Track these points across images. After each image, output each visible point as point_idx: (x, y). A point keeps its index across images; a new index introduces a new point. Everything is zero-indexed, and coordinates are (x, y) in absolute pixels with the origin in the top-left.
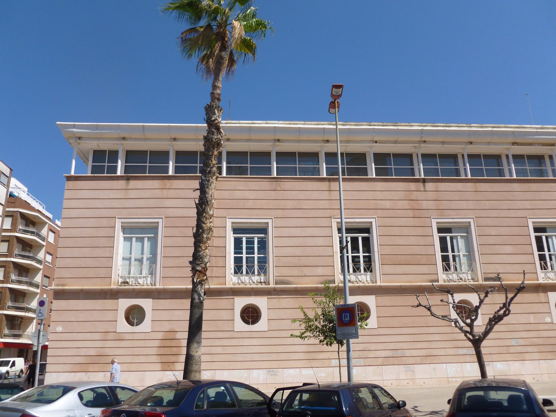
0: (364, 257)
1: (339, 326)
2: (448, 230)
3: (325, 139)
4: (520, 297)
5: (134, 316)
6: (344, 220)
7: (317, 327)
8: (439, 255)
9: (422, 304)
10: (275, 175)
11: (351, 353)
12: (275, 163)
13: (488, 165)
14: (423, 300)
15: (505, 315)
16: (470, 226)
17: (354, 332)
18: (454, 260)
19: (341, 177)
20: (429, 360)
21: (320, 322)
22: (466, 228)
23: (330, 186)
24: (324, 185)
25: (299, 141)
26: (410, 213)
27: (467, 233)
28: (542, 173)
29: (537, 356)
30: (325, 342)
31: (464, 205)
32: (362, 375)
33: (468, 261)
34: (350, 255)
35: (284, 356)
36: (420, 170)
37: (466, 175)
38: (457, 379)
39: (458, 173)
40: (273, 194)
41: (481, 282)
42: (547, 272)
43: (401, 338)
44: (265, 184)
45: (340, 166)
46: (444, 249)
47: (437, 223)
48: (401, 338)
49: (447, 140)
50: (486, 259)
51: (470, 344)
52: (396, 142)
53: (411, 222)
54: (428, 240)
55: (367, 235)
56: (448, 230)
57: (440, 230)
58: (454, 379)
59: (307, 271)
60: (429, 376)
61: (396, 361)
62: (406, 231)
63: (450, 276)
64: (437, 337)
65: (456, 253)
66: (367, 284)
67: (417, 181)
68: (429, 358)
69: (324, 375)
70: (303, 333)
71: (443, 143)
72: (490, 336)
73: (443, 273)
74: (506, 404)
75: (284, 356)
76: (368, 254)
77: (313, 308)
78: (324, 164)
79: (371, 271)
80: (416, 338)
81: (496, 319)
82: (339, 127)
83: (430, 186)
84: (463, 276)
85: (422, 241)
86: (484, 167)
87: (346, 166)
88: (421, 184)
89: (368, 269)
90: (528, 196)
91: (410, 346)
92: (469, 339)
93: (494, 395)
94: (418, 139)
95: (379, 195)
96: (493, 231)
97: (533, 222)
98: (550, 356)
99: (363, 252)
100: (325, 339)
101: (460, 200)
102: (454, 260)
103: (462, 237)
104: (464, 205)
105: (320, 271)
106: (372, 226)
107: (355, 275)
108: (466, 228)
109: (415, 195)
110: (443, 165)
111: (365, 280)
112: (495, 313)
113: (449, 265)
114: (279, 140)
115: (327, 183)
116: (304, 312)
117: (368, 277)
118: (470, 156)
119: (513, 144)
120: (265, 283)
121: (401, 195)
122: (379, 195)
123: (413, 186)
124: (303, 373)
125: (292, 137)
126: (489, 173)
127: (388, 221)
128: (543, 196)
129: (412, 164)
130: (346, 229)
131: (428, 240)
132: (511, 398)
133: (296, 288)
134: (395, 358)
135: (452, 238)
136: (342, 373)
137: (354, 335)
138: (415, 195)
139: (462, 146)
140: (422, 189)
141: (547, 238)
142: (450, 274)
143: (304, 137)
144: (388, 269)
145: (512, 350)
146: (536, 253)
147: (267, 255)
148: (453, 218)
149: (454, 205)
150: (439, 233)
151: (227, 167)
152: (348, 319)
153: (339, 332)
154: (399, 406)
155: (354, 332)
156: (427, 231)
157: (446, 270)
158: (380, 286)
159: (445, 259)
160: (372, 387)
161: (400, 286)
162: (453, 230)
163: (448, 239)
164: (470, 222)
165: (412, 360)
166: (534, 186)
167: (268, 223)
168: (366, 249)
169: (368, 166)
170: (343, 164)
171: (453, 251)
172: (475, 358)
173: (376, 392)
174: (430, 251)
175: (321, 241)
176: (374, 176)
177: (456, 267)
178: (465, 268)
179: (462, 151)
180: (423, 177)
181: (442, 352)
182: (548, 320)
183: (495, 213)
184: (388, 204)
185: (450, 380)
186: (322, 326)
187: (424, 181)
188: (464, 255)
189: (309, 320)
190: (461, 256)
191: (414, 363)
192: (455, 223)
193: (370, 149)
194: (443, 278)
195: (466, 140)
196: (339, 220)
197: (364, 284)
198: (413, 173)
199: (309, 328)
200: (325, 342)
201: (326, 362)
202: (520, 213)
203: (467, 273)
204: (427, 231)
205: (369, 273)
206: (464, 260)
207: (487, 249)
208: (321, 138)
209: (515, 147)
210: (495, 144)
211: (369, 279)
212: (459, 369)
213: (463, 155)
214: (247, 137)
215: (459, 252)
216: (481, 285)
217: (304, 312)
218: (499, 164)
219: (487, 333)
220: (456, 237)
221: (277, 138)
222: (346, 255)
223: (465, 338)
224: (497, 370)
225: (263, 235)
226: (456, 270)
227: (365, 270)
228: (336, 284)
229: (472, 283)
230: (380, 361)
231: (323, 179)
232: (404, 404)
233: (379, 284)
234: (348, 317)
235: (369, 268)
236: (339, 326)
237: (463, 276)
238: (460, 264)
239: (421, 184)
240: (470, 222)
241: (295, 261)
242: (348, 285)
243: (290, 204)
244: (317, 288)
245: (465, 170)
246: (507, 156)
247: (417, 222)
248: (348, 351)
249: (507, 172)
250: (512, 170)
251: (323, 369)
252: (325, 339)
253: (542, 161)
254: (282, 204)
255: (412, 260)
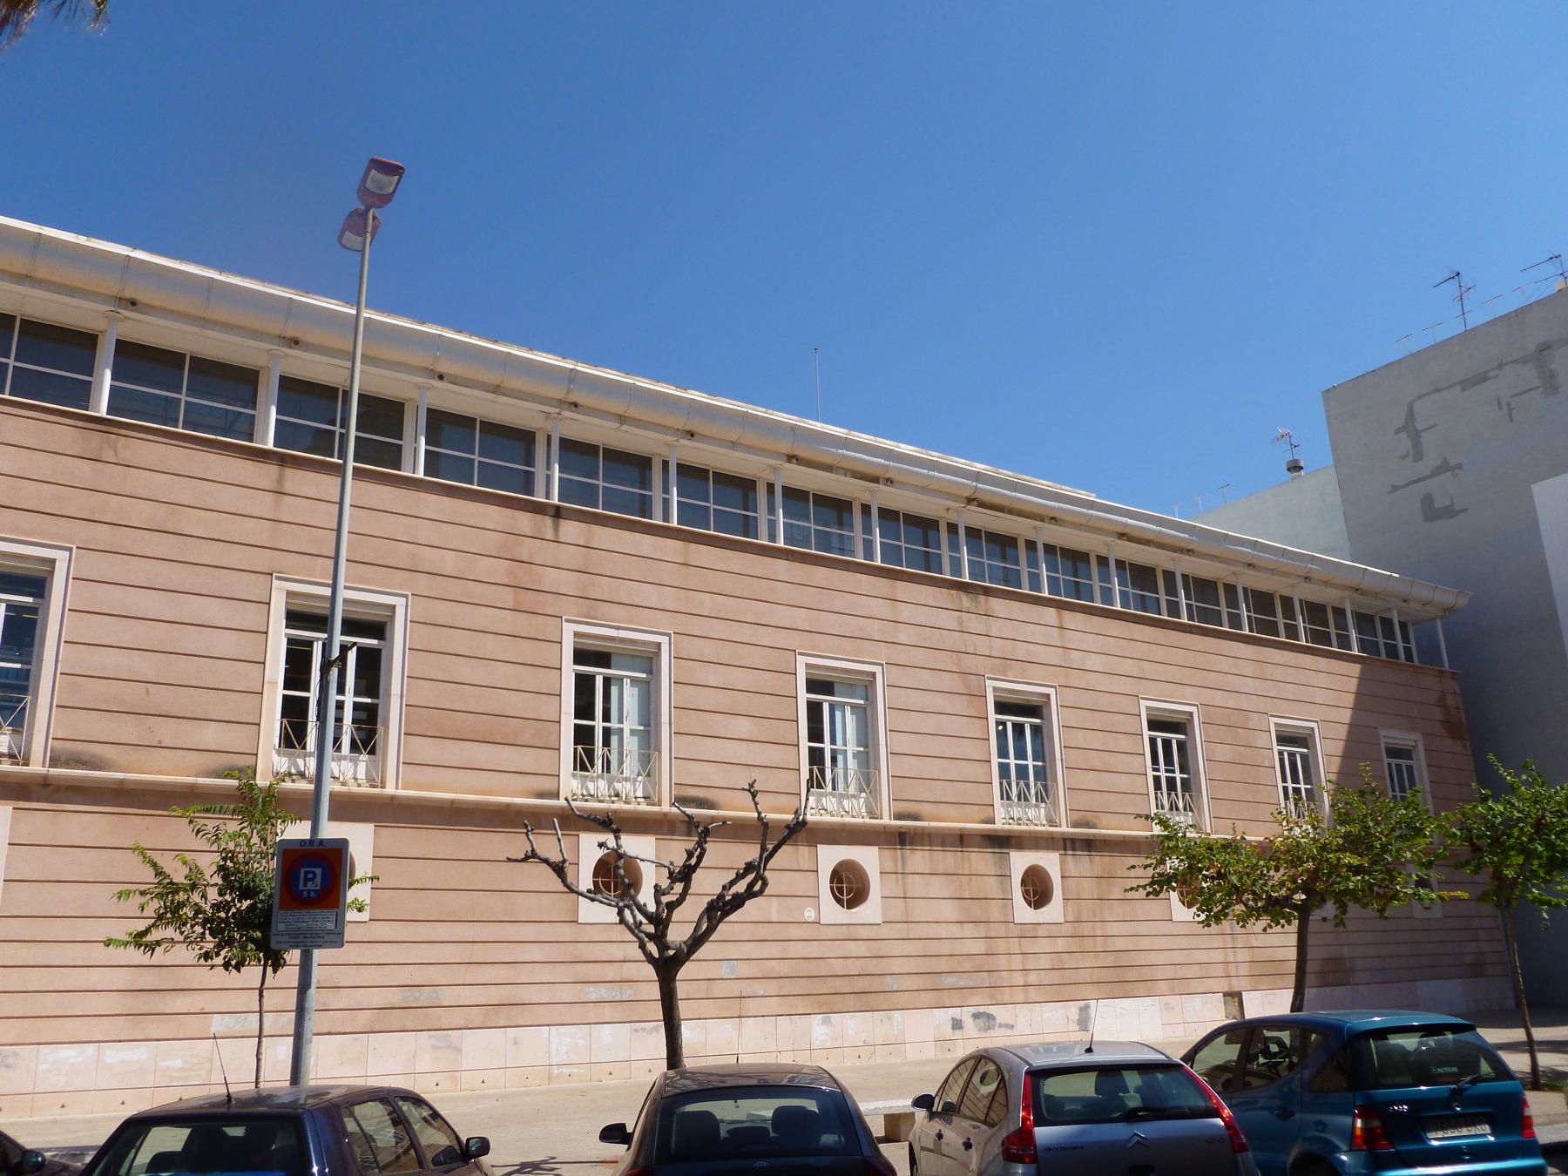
0: (356, 706)
1: (282, 907)
2: (602, 659)
3: (290, 333)
4: (785, 855)
5: (1037, 890)
6: (343, 594)
7: (198, 911)
8: (569, 722)
9: (540, 852)
10: (103, 411)
11: (312, 992)
12: (108, 374)
13: (723, 502)
14: (547, 845)
15: (750, 894)
16: (658, 654)
17: (331, 926)
18: (606, 743)
19: (351, 464)
20: (504, 1016)
21: (204, 896)
22: (865, 685)
23: (280, 480)
24: (265, 474)
25: (203, 322)
26: (508, 597)
27: (650, 672)
28: (1011, 578)
29: (772, 1005)
30: (219, 960)
31: (650, 595)
32: (337, 1065)
33: (640, 747)
34: (349, 699)
35: (50, 1004)
36: (551, 481)
37: (666, 518)
38: (574, 1070)
39: (644, 508)
40: (84, 471)
41: (666, 807)
42: (821, 795)
43: (436, 953)
44: (63, 435)
45: (353, 433)
46: (584, 708)
47: (576, 634)
48: (436, 953)
49: (635, 412)
50: (686, 746)
51: (649, 971)
52: (496, 389)
53: (510, 622)
54: (543, 680)
55: (375, 642)
56: (602, 659)
57: (581, 656)
58: (566, 1070)
59: (165, 731)
60: (548, 1060)
61: (409, 1019)
62: (489, 646)
63: (591, 785)
64: (535, 952)
65: (614, 724)
66: (355, 789)
67: (539, 509)
68: (504, 1012)
69: (178, 1063)
70: (147, 931)
71: (622, 419)
72: (704, 951)
73: (574, 776)
74: (723, 1134)
75: (50, 1004)
76: (369, 700)
77: (194, 850)
78: (274, 409)
79: (372, 752)
80: (478, 953)
81: (720, 908)
82: (366, 314)
83: (571, 530)
84: (624, 788)
85: (530, 679)
86: (476, 458)
87: (337, 429)
88: (548, 521)
89: (365, 743)
90: (806, 596)
91: (459, 975)
92: (650, 958)
93: (727, 1112)
94: (557, 393)
95: (426, 532)
96: (713, 676)
97: (808, 665)
98: (801, 1005)
99: (356, 694)
100: (220, 947)
101: (643, 581)
102: (606, 743)
103: (634, 680)
104: (650, 595)
105: (210, 735)
106: (392, 617)
107: (289, 756)
108: (648, 660)
109: (527, 549)
110: (613, 479)
111: (350, 774)
112: (724, 888)
113: (590, 754)
114: (133, 303)
115: (270, 471)
116: (154, 865)
117: (362, 767)
118: (684, 469)
119: (790, 458)
120: (12, 756)
121: (492, 541)
122: (426, 532)
123: (524, 521)
124: (109, 1060)
125: (181, 305)
126: (723, 522)
127: (442, 612)
128: (839, 602)
129: (529, 461)
130: (345, 622)
131: (543, 680)
132: (779, 1113)
133: (122, 781)
134: (409, 1013)
135: (607, 681)
136: (263, 1057)
137: (327, 938)
138: (527, 549)
139: (670, 439)
140: (550, 535)
141: (832, 707)
142: (592, 780)
143: (221, 313)
144: (426, 749)
145: (719, 989)
146: (805, 744)
147: (33, 667)
148: (618, 628)
149: (625, 592)
150: (576, 662)
151: (114, 391)
152: (315, 885)
153: (281, 927)
154: (470, 1152)
155: (331, 926)
156: (543, 653)
157: (584, 768)
158: (393, 798)
159: (583, 736)
160: (396, 1102)
161: (452, 802)
162: (614, 659)
163: (826, 707)
164: (659, 645)
165: (457, 1017)
166: (821, 574)
167: (53, 561)
168: (363, 683)
169: (406, 443)
170: (1188, 597)
171: (606, 718)
172: (657, 1011)
173: (405, 1108)
174: (545, 708)
175: (226, 643)
176: (420, 474)
177: (609, 762)
178: (631, 765)
179: (665, 452)
180: (556, 501)
181: (543, 994)
182: (810, 914)
183: (722, 630)
184: (449, 563)
185: (555, 1071)
186: (213, 906)
187: (558, 513)
188: (633, 732)
189: (174, 888)
190: (626, 733)
191: (462, 1024)
192: (623, 640)
193: (421, 395)
194: (571, 787)
195: (680, 422)
196: (327, 592)
197: (344, 789)
198: (528, 484)
199: (171, 914)
200: (219, 960)
201: (193, 1025)
202: (781, 639)
203: (635, 780)
204: (543, 653)
205: (364, 757)
206: (631, 744)
207: (692, 722)
208: (275, 328)
209: (793, 466)
210: (749, 449)
211: (361, 775)
212: (581, 1042)
213: (666, 464)
214: (19, 267)
215: (621, 721)
216: (665, 814)
217: (154, 865)
218: (748, 503)
219: (697, 941)
220: (621, 679)
221: (129, 293)
222: (334, 697)
223: (640, 955)
224: (713, 1043)
225: (30, 600)
226: (608, 770)
227: (354, 747)
228: (562, 802)
229: (644, 807)
230: (363, 1019)
231: (262, 455)
232: (484, 1146)
233: (390, 790)
234: (318, 880)
235: (367, 737)
236: (282, 907)
237: (623, 787)
238: (621, 753)
239: (548, 521)
240: (659, 645)
241: (133, 695)
242: (329, 786)
243: (141, 513)
244: (193, 787)
245: (666, 503)
246: (771, 487)
247: (522, 624)
248: (304, 986)
249: (763, 528)
250: (776, 524)
251: (219, 1043)
252: (220, 947)
253: (845, 515)
254: (114, 507)
255: (495, 731)
